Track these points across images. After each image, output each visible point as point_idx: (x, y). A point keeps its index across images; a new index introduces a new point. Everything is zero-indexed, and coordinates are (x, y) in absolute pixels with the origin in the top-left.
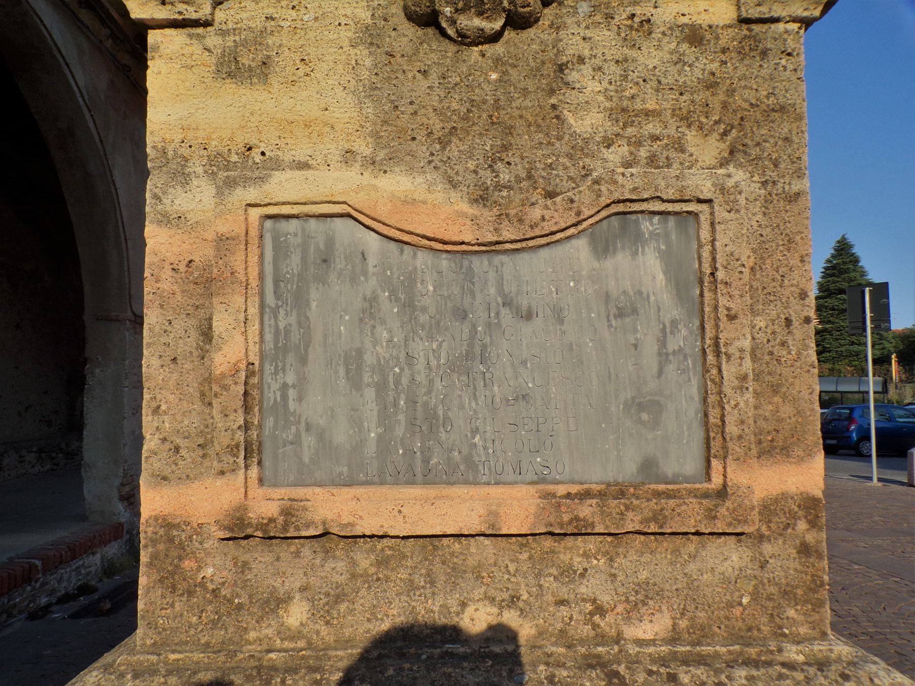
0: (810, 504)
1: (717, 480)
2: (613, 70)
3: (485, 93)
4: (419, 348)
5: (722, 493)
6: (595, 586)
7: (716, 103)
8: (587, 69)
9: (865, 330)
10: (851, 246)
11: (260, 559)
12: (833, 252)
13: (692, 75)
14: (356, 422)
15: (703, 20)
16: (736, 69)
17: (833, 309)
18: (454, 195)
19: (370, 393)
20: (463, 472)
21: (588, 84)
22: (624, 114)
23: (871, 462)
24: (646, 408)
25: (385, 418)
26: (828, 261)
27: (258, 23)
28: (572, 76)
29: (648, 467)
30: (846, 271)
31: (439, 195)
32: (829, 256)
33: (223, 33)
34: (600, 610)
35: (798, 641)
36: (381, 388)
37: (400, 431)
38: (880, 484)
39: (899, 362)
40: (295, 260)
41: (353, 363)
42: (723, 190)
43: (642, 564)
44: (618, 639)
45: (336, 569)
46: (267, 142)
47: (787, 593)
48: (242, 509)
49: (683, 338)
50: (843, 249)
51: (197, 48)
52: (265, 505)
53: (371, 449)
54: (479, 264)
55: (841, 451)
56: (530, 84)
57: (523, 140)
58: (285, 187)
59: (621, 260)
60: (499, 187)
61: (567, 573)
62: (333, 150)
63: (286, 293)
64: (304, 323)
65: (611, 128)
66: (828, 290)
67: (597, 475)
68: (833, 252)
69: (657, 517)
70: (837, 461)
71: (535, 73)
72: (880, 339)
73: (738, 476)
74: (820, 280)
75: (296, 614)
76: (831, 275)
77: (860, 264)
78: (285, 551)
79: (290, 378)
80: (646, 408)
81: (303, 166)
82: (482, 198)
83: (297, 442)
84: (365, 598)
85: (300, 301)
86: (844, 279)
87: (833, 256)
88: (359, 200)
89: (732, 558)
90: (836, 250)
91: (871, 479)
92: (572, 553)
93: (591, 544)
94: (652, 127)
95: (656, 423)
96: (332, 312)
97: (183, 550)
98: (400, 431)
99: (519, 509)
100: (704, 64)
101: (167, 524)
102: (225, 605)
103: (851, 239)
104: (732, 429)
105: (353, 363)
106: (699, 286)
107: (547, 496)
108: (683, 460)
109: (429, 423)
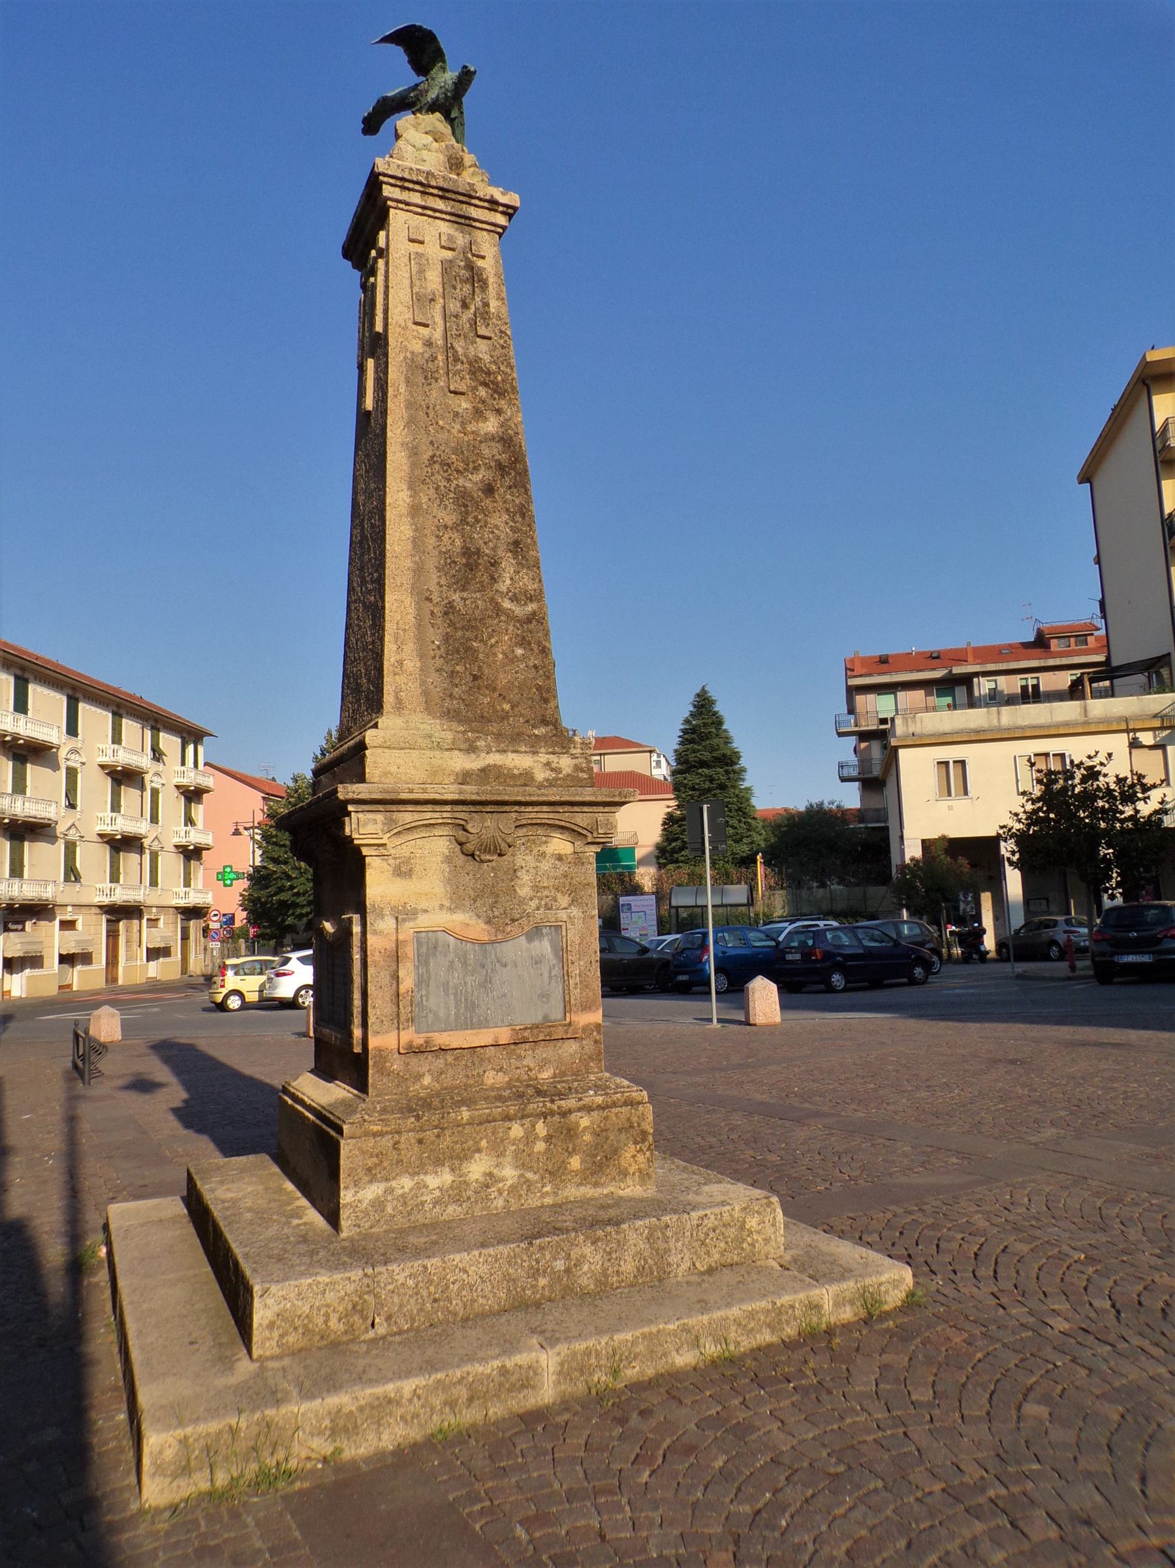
0: (598, 1026)
1: (568, 1020)
2: (532, 870)
3: (489, 881)
4: (468, 979)
5: (570, 1024)
6: (528, 1061)
7: (567, 883)
8: (524, 871)
9: (704, 853)
10: (713, 702)
11: (414, 1061)
12: (692, 709)
13: (559, 873)
14: (447, 1008)
15: (563, 852)
16: (574, 870)
17: (693, 789)
18: (479, 921)
19: (452, 997)
20: (483, 1024)
21: (525, 877)
22: (536, 888)
23: (710, 1000)
24: (545, 996)
25: (457, 1007)
26: (687, 721)
27: (407, 855)
28: (519, 874)
29: (546, 1017)
30: (708, 736)
31: (473, 921)
32: (687, 714)
33: (395, 858)
34: (530, 1070)
35: (593, 1073)
36: (455, 995)
37: (462, 1011)
38: (719, 1026)
39: (767, 863)
40: (424, 949)
41: (446, 986)
42: (570, 918)
43: (544, 1052)
44: (536, 1079)
45: (440, 1063)
46: (412, 904)
47: (590, 1058)
48: (411, 1042)
49: (556, 971)
50: (704, 705)
51: (385, 864)
52: (419, 1040)
53: (452, 1017)
54: (488, 947)
55: (695, 989)
56: (504, 877)
57: (502, 899)
58: (423, 922)
59: (536, 944)
60: (494, 917)
61: (519, 1057)
62: (436, 904)
63: (423, 960)
64: (428, 972)
65: (532, 894)
66: (686, 762)
67: (529, 1021)
68: (692, 709)
69: (549, 1034)
70: (681, 1002)
71: (506, 873)
72: (749, 830)
73: (575, 1018)
74: (677, 747)
75: (427, 1080)
76: (692, 741)
77: (724, 727)
78: (422, 1057)
79: (424, 993)
80: (545, 996)
81: (426, 911)
82: (489, 922)
83: (426, 1016)
84: (451, 1072)
85: (427, 963)
86: (705, 747)
87: (692, 715)
88: (449, 926)
89: (572, 1047)
90: (695, 706)
91: (710, 1020)
92: (521, 1050)
93: (527, 1046)
94: (546, 893)
95: (548, 1001)
96: (438, 967)
97: (385, 1059)
98: (462, 1011)
99: (504, 1035)
100: (563, 868)
101: (379, 1050)
102: (401, 1079)
103: (713, 693)
104: (573, 1002)
105: (446, 986)
106: (561, 952)
107: (513, 1030)
108: (556, 1014)
109: (472, 1006)
